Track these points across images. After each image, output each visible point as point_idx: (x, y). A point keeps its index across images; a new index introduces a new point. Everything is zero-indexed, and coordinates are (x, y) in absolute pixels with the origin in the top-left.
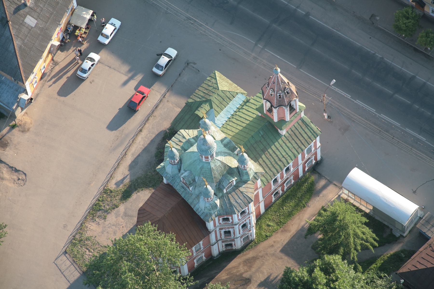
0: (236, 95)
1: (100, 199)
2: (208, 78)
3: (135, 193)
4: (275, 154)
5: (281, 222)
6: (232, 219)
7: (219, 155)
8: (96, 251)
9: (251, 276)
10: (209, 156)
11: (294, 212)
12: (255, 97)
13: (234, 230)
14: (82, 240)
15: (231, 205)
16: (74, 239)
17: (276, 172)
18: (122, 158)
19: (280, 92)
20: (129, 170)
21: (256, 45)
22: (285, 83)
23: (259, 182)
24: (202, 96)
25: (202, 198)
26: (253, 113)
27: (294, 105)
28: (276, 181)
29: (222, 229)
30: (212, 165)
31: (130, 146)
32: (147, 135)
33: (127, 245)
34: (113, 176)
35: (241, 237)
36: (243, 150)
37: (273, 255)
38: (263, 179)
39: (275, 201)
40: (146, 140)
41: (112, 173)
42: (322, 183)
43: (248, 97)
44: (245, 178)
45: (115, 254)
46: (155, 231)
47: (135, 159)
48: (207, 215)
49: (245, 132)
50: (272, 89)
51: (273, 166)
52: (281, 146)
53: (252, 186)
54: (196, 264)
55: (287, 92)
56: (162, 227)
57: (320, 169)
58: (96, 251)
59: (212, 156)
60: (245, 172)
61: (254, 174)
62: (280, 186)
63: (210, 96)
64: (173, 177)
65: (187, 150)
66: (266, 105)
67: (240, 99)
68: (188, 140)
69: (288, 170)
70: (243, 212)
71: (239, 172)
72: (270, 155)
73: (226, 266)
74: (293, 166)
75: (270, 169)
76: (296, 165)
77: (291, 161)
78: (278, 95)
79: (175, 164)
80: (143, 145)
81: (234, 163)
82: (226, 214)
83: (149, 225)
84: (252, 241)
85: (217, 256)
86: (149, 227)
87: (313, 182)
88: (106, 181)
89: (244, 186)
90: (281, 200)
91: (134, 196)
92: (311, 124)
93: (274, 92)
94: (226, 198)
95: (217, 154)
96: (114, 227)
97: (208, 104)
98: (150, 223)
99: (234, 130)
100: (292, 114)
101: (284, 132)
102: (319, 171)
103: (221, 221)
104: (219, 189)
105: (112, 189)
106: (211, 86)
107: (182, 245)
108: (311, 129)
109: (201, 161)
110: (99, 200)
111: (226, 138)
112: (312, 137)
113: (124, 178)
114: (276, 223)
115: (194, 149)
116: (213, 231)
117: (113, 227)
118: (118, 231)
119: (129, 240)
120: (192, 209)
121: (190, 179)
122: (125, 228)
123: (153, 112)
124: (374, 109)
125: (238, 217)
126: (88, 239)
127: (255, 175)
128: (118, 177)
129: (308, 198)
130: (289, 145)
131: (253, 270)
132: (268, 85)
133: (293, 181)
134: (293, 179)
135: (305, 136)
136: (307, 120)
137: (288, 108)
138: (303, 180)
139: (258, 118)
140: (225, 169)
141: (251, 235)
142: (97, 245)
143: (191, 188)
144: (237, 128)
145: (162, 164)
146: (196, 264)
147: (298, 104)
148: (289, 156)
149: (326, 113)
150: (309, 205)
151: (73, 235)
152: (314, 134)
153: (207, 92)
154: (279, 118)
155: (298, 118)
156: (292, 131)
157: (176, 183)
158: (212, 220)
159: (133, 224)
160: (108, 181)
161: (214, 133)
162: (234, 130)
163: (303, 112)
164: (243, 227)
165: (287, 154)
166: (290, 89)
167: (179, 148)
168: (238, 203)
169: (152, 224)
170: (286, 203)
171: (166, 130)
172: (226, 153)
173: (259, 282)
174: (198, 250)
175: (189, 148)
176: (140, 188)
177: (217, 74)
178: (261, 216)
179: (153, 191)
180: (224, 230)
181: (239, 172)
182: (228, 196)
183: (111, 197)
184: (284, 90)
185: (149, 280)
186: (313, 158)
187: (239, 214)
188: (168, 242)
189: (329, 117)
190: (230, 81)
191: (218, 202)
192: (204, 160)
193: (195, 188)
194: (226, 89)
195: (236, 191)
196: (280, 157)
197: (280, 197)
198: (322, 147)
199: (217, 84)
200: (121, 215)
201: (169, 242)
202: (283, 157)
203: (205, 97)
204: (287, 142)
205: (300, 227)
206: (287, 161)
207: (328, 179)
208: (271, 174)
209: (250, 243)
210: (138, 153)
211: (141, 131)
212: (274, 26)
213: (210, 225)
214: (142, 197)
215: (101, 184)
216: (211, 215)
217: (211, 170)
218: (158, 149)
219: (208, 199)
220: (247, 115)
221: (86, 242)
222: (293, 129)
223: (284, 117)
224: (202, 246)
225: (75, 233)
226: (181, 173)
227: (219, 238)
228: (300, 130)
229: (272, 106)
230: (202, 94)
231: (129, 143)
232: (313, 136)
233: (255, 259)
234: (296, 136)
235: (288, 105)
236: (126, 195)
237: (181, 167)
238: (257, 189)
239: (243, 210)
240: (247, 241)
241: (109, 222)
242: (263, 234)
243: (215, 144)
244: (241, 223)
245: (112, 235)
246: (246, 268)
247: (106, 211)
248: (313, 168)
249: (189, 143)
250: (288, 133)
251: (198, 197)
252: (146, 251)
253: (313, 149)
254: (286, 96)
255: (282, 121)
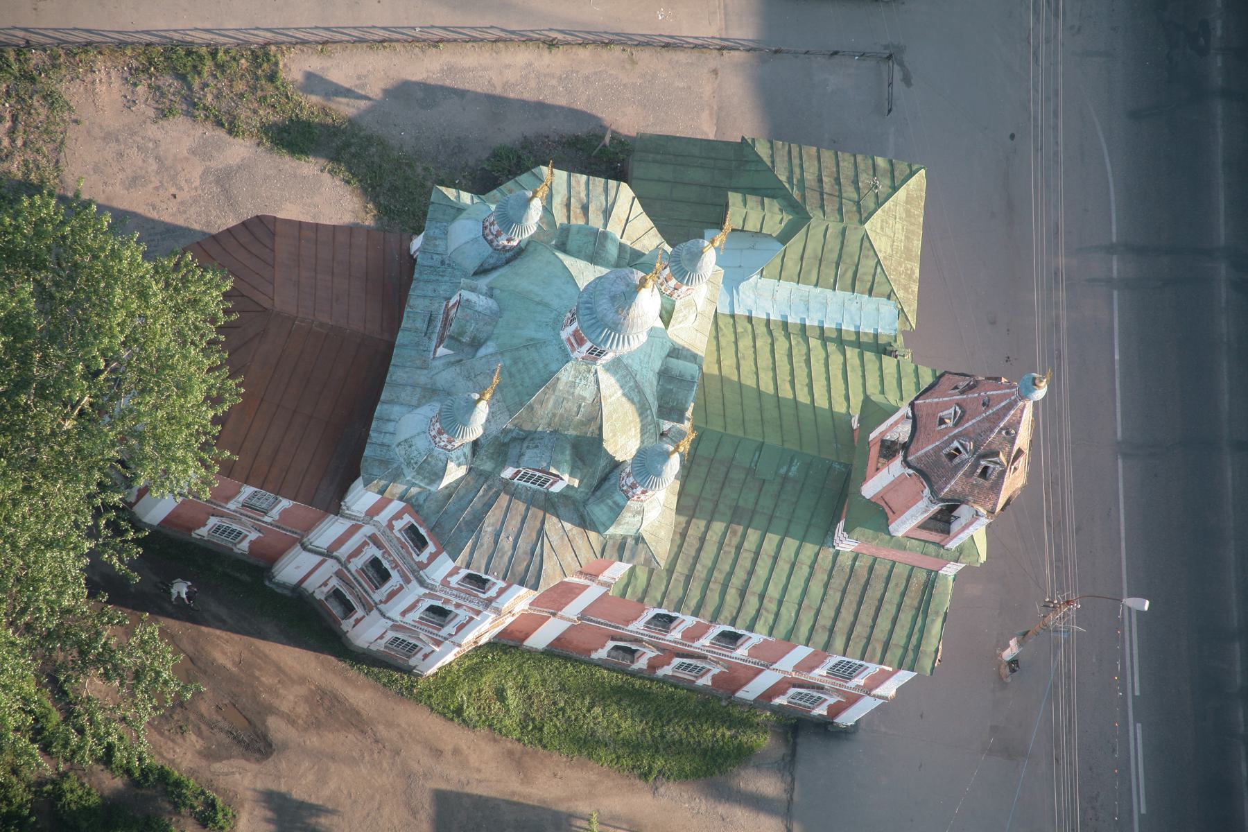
0: (882, 295)
1: (221, 54)
2: (881, 162)
3: (322, 162)
4: (754, 562)
5: (541, 730)
6: (432, 557)
7: (614, 373)
8: (30, 156)
9: (285, 746)
10: (588, 345)
11: (602, 752)
12: (908, 368)
13: (401, 588)
14: (33, 80)
15: (475, 523)
16: (19, 51)
17: (693, 602)
18: (417, 40)
19: (970, 446)
20: (386, 92)
21: (1111, 249)
22: (1013, 441)
23: (617, 571)
24: (802, 180)
25: (429, 410)
26: (847, 398)
27: (963, 521)
28: (665, 622)
29: (379, 545)
30: (566, 375)
31: (475, 40)
32: (552, 76)
33: (95, 257)
34: (329, 47)
35: (396, 627)
36: (685, 446)
37: (408, 775)
38: (642, 576)
39: (599, 664)
40: (533, 84)
41: (339, 37)
42: (768, 785)
43: (900, 339)
44: (598, 511)
45: (39, 234)
46: (213, 320)
47: (442, 88)
48: (385, 463)
49: (761, 409)
50: (964, 412)
51: (708, 582)
52: (793, 565)
53: (586, 555)
54: (203, 532)
55: (986, 468)
56: (241, 339)
57: (809, 748)
58: (30, 156)
59: (596, 353)
60: (618, 497)
61: (632, 532)
62: (658, 647)
63: (822, 207)
64: (446, 265)
65: (565, 251)
66: (896, 423)
67: (874, 316)
68: (605, 235)
69: (731, 639)
70: (479, 582)
71: (605, 479)
72: (739, 548)
73: (263, 637)
74: (755, 650)
75: (688, 578)
76: (767, 657)
77: (766, 630)
78: (956, 444)
79: (490, 243)
80: (505, 85)
81: (623, 441)
82: (437, 525)
83: (218, 287)
84: (409, 671)
85: (283, 585)
86: (212, 291)
87: (751, 750)
88: (300, 35)
89: (568, 526)
90: (616, 679)
91: (310, 167)
92: (940, 620)
93: (956, 425)
94: (486, 491)
95: (617, 366)
96: (153, 166)
97: (787, 218)
98: (228, 286)
99: (747, 366)
100: (925, 535)
101: (846, 544)
102: (801, 750)
103: (399, 525)
104: (501, 446)
105: (282, 74)
106: (858, 189)
107: (222, 447)
108: (922, 631)
109: (557, 325)
110: (214, 54)
111: (694, 358)
112: (895, 653)
113: (347, 93)
114: (526, 715)
115: (585, 273)
116: (349, 517)
117: (151, 160)
118: (150, 187)
119: (115, 255)
120: (376, 400)
121: (471, 328)
122: (173, 206)
123: (646, 43)
124: (1147, 803)
125: (451, 574)
126: (51, 99)
127: (630, 542)
128: (342, 69)
129: (681, 770)
130: (816, 589)
131: (313, 740)
132: (970, 388)
133: (706, 681)
134: (714, 678)
135: (884, 624)
136: (944, 598)
137: (937, 507)
138: (736, 712)
139: (839, 423)
140: (582, 423)
141: (426, 656)
142: (51, 146)
143: (442, 351)
144: (757, 372)
145: (466, 197)
146: (203, 532)
147: (974, 533)
148: (777, 614)
149: (1020, 644)
150: (662, 790)
151: (33, 38)
152: (911, 654)
153: (827, 188)
154: (882, 495)
155: (929, 563)
156: (871, 569)
157: (431, 287)
158: (382, 492)
159: (208, 223)
160: (304, 42)
161: (687, 306)
162: (747, 366)
163: (960, 566)
164: (432, 609)
165: (780, 603)
166: (1002, 475)
167: (560, 217)
168: (496, 542)
169: (227, 296)
170: (618, 703)
171: (604, 129)
172: (641, 392)
173: (283, 789)
174: (252, 508)
175: (577, 254)
176: (350, 170)
177: (918, 181)
178: (516, 647)
179: (369, 221)
180: (378, 554)
181: (605, 482)
182: (497, 495)
183: (254, 89)
184: (984, 456)
185: (26, 408)
186: (832, 700)
187: (464, 572)
188: (198, 389)
189: (1014, 662)
190: (917, 244)
191: (455, 473)
192: (566, 333)
193: (453, 364)
194: (881, 245)
195: (532, 510)
196: (756, 586)
197: (623, 671)
198: (886, 708)
199: (879, 205)
200: (212, 164)
201: (201, 398)
202: (762, 597)
203: (808, 193)
204: (820, 577)
205: (563, 807)
206: (755, 620)
207: (796, 797)
208: (676, 592)
209: (398, 669)
210: (467, 87)
211: (552, 44)
212: (1223, 270)
213: (361, 498)
214: (322, 198)
215: (277, 23)
216: (396, 476)
217: (547, 378)
218: (526, 144)
219: (440, 433)
220: (828, 379)
221: (36, 101)
222: (881, 570)
223: (897, 513)
224: (275, 513)
225: (42, 40)
226: (473, 282)
227: (343, 552)
228: (892, 596)
229: (905, 447)
230: (810, 176)
231: (481, 29)
232: (899, 652)
233: (355, 721)
234: (862, 597)
235: (943, 500)
236: (294, 137)
237: (494, 268)
238: (593, 576)
239: (484, 577)
240: (398, 655)
241: (159, 135)
242: (461, 695)
243: (643, 338)
244: (439, 598)
245: (120, 176)
246: (302, 710)
247: (192, 106)
248: (799, 720)
249: (594, 246)
250: (855, 559)
251: (431, 392)
252: (113, 336)
253: (859, 681)
254: (971, 473)
255: (878, 516)
